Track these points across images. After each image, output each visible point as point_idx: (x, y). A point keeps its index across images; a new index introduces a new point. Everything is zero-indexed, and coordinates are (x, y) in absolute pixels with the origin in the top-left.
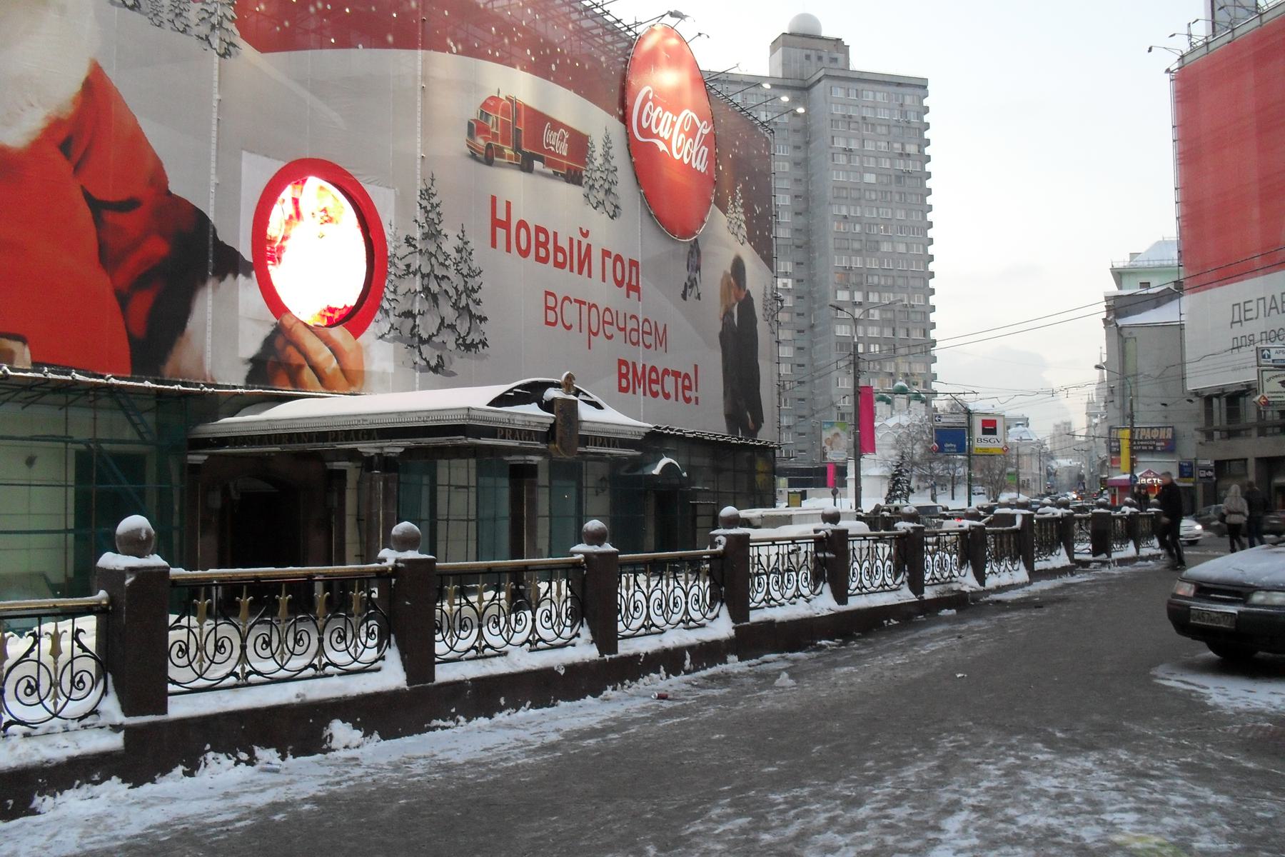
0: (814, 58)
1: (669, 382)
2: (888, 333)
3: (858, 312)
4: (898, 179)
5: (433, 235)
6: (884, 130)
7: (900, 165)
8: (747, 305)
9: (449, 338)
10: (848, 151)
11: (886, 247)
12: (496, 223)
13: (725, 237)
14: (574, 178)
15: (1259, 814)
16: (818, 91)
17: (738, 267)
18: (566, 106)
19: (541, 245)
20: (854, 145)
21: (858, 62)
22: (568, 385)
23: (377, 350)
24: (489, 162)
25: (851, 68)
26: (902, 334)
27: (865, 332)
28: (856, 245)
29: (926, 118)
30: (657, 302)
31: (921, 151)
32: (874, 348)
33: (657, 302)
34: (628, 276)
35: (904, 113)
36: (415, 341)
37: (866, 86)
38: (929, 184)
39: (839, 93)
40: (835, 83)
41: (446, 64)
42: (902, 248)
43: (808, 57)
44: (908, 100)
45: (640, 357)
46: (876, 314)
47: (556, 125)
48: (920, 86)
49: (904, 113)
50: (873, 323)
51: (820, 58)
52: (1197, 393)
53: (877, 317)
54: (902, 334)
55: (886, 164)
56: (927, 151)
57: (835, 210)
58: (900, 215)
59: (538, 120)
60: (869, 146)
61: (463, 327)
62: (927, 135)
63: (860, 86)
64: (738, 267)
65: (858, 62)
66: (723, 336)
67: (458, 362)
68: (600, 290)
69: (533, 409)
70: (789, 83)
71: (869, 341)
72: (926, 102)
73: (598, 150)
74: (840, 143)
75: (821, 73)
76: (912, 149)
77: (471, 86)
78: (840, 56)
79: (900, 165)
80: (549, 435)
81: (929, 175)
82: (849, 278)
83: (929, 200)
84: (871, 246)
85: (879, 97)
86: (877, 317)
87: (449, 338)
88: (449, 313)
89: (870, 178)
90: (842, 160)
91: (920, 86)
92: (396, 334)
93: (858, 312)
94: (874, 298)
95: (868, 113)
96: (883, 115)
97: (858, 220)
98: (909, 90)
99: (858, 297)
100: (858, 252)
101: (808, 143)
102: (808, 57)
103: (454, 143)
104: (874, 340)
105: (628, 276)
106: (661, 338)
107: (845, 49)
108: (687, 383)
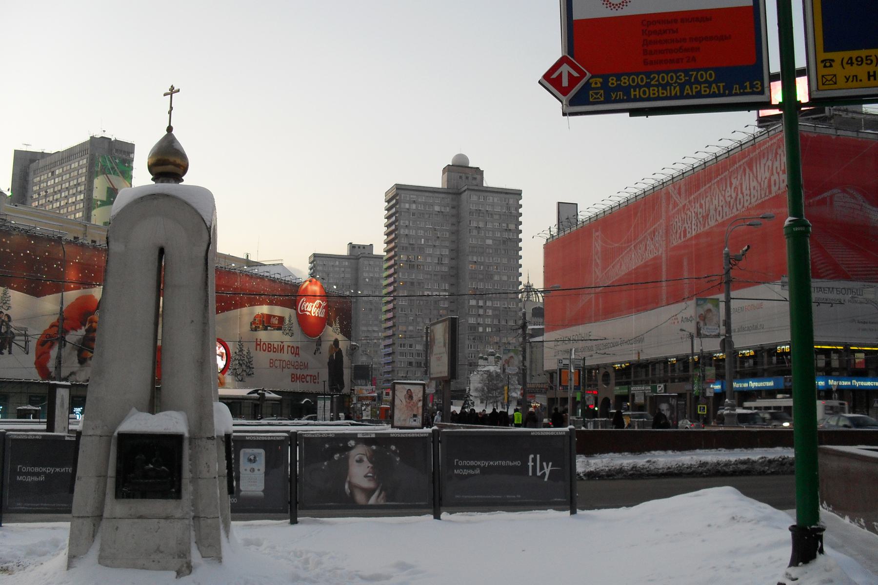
0: (464, 177)
1: (308, 378)
2: (496, 322)
3: (481, 312)
4: (504, 242)
5: (241, 350)
6: (497, 217)
7: (506, 235)
8: (339, 353)
9: (244, 373)
10: (478, 228)
11: (496, 278)
12: (257, 345)
13: (332, 333)
14: (279, 329)
15: (53, 353)
16: (465, 196)
17: (336, 342)
18: (278, 311)
19: (270, 348)
20: (481, 225)
21: (489, 181)
22: (263, 390)
23: (228, 378)
24: (256, 330)
25: (485, 185)
26: (503, 323)
27: (484, 321)
28: (481, 276)
29: (520, 210)
30: (306, 356)
31: (517, 227)
32: (488, 330)
33: (306, 356)
34: (295, 351)
35: (508, 208)
36: (236, 375)
37: (489, 194)
38: (520, 244)
39: (474, 198)
40: (473, 193)
41: (245, 310)
42: (505, 278)
43: (461, 177)
44: (511, 201)
45: (299, 372)
46: (490, 312)
47: (274, 316)
48: (518, 194)
49: (508, 208)
50: (488, 316)
51: (467, 178)
52: (547, 371)
53: (490, 314)
54: (503, 323)
55: (498, 235)
56: (520, 227)
57: (470, 258)
58: (505, 261)
59: (269, 317)
60: (489, 226)
61: (248, 370)
62: (520, 219)
63: (486, 194)
64: (336, 342)
65: (489, 181)
66: (329, 364)
67: (247, 379)
68: (286, 356)
69: (256, 395)
70: (450, 191)
71: (485, 326)
72: (520, 202)
73: (287, 322)
74: (474, 224)
75: (466, 187)
76: (512, 227)
77: (251, 314)
78: (478, 177)
79: (506, 235)
80: (258, 399)
81: (521, 240)
82: (479, 295)
83: (520, 253)
84: (489, 277)
85: (496, 200)
86: (490, 314)
87: (244, 373)
88: (244, 367)
89: (489, 242)
90: (475, 232)
91: (518, 194)
92: (232, 374)
93: (481, 312)
94: (489, 303)
95: (489, 208)
96: (498, 209)
97: (481, 264)
98: (511, 196)
99: (481, 303)
100: (481, 280)
101: (459, 222)
102: (461, 177)
103: (247, 328)
104: (489, 326)
105: (295, 351)
106: (306, 367)
107: (481, 173)
108: (314, 378)
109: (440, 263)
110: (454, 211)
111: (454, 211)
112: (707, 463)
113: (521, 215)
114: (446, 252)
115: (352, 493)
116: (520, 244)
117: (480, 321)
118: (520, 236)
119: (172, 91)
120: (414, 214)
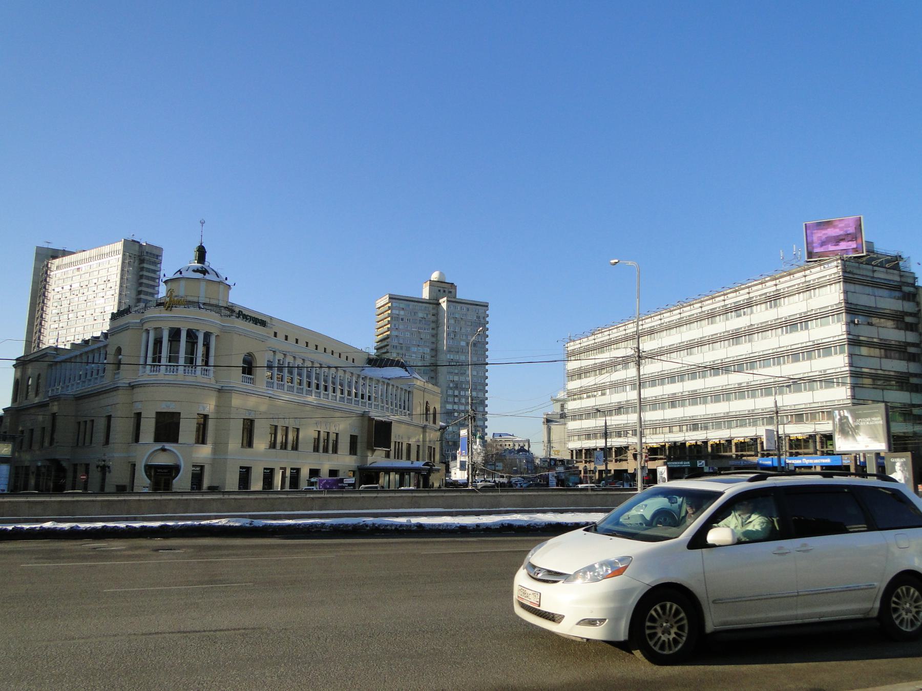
3: (456, 400)
49: (478, 317)
60: (463, 331)
78: (453, 291)
93: (456, 400)
101: (438, 327)
109: (423, 358)
110: (433, 318)
111: (433, 318)
112: (367, 526)
113: (488, 323)
114: (427, 350)
115: (684, 517)
116: (487, 346)
117: (456, 407)
118: (487, 340)
119: (203, 223)
120: (402, 319)
